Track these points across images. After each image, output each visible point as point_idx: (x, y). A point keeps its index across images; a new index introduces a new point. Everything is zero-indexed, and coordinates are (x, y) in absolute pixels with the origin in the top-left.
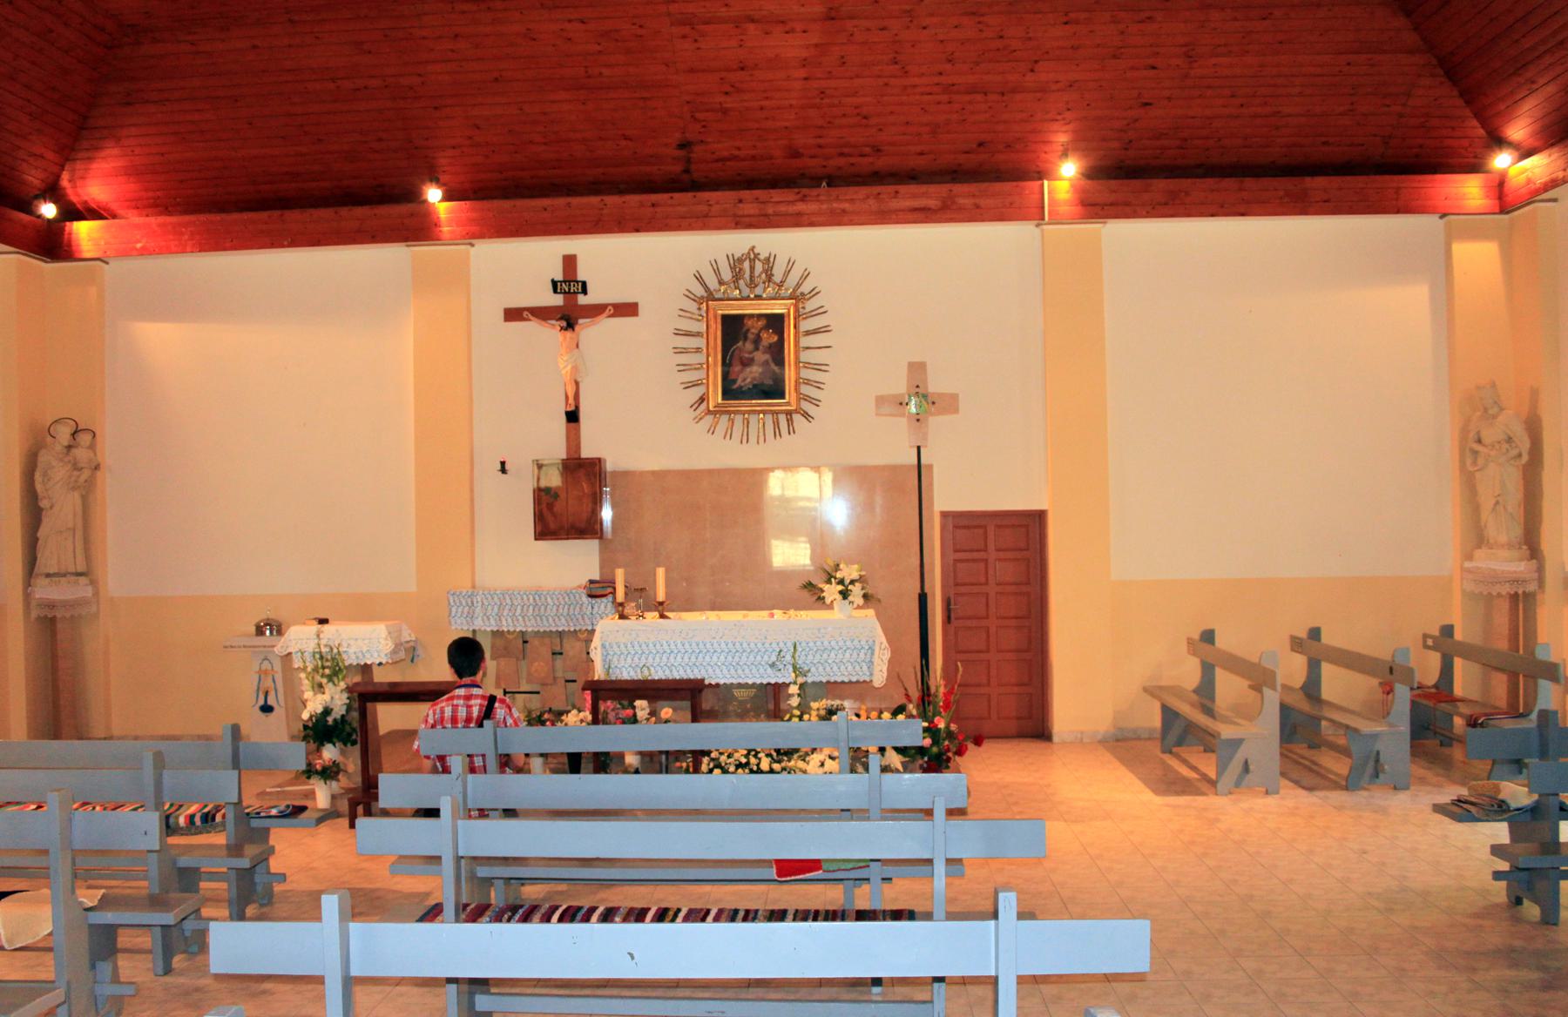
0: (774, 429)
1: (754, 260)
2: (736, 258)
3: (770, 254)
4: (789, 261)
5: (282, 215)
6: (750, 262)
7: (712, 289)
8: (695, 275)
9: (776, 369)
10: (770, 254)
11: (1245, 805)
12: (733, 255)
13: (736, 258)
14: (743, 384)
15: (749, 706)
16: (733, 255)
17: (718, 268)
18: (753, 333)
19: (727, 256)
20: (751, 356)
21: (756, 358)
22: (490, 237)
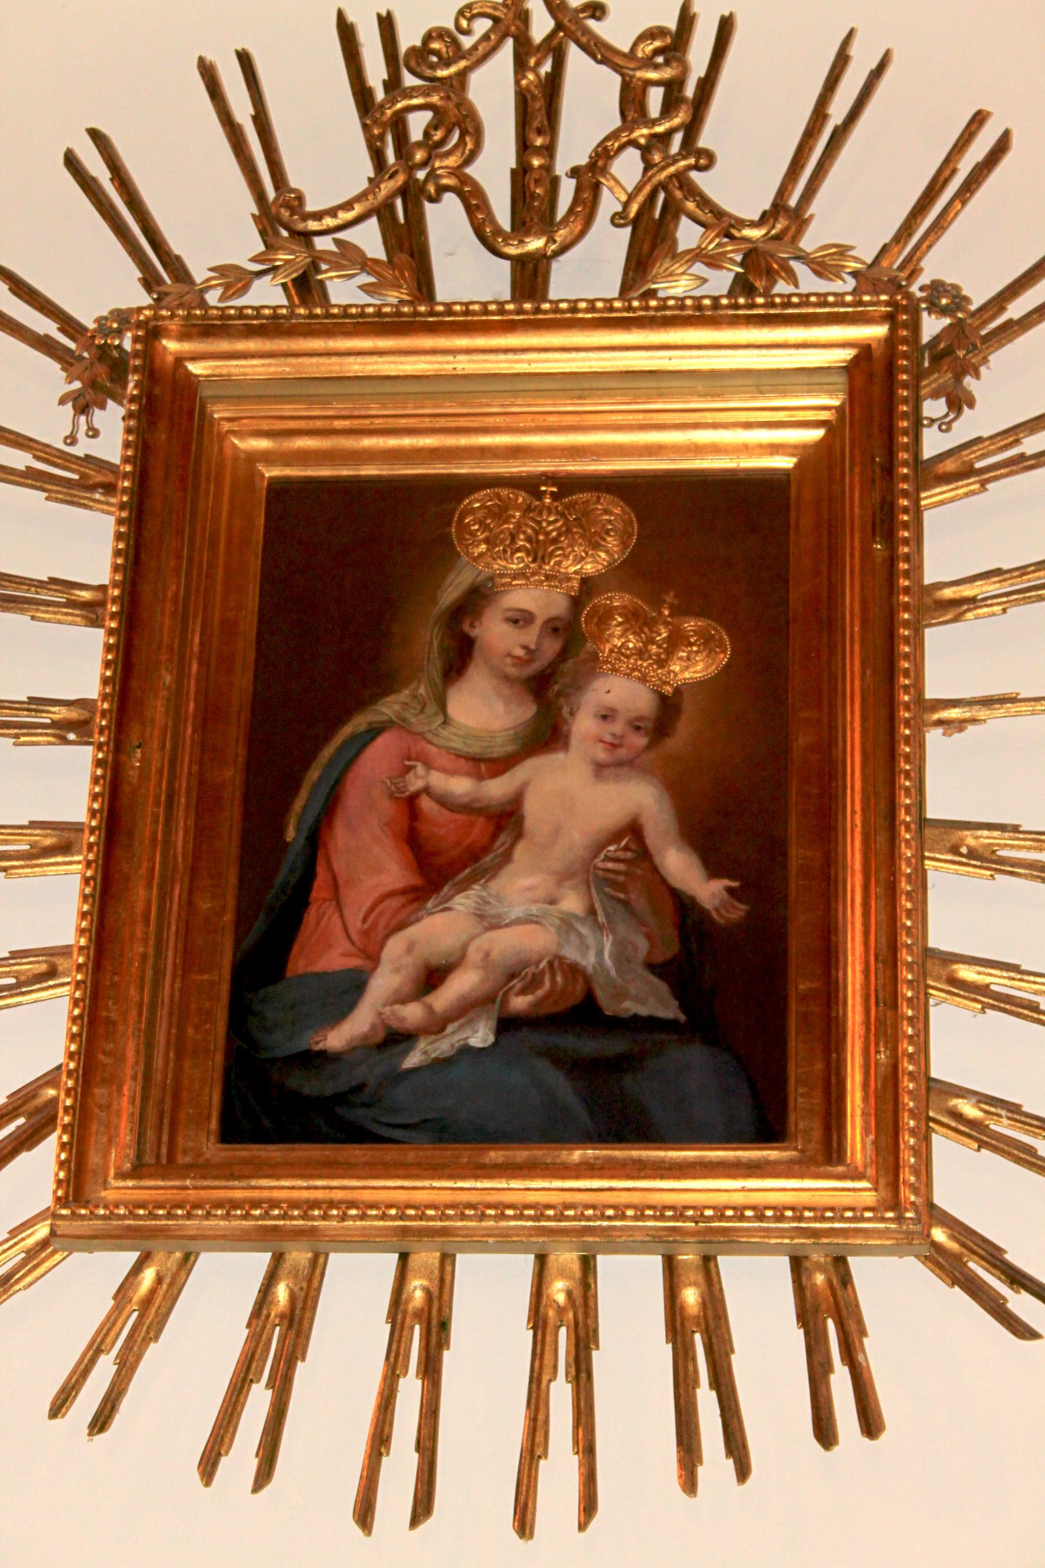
0: (95, 1350)
1: (553, 47)
2: (408, 39)
3: (686, 20)
4: (842, 60)
5: (100, 1107)
6: (520, 65)
7: (199, 274)
8: (71, 161)
9: (520, 50)
10: (686, 20)
11: (438, 1052)
12: (387, 24)
13: (408, 39)
14: (412, 1013)
15: (944, 301)
16: (387, 24)
17: (262, 121)
18: (520, 619)
19: (347, 33)
20: (497, 788)
21: (532, 809)
22: (539, 1142)
